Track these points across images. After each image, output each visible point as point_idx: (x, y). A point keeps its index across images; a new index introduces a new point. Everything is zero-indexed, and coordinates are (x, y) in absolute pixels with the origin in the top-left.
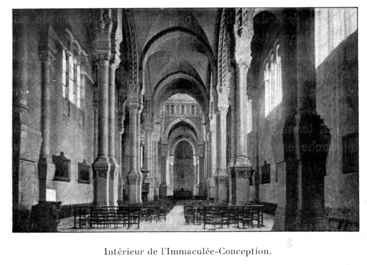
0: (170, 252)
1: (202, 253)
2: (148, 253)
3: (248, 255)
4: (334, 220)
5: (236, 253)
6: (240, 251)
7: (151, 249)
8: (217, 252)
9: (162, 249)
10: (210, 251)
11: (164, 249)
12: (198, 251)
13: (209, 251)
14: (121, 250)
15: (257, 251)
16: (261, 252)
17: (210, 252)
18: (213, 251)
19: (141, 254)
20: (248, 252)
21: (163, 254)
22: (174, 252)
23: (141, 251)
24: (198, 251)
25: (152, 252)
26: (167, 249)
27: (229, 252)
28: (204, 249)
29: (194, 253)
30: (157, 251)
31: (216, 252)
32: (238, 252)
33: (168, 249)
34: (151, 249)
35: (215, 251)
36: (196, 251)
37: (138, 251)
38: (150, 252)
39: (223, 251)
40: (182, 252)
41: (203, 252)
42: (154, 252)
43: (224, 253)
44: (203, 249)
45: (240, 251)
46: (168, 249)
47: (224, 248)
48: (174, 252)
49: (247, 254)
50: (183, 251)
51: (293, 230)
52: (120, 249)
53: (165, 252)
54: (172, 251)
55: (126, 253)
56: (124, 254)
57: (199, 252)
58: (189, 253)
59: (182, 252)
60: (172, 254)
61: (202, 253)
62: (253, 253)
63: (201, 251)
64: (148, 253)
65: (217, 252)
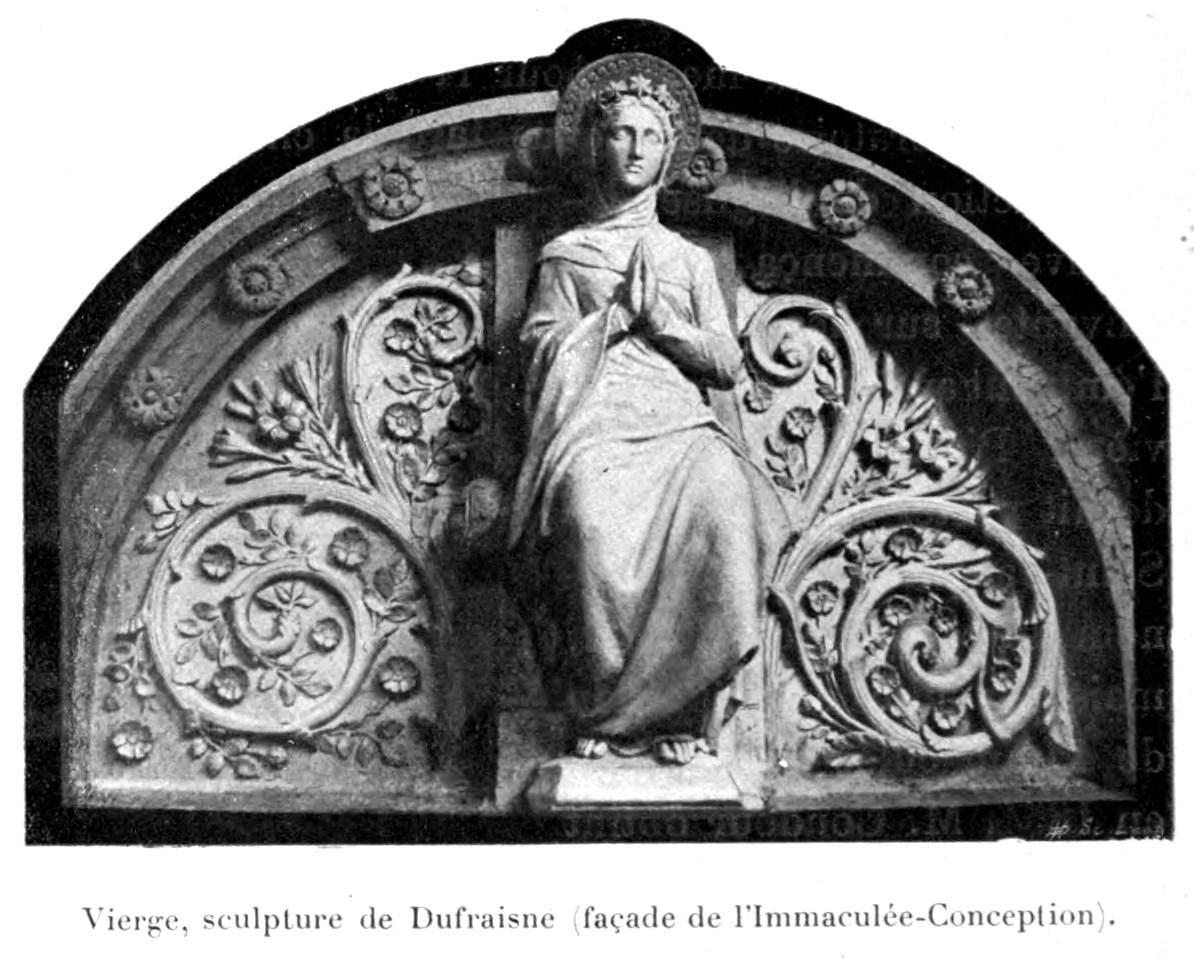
0: (764, 920)
1: (872, 920)
2: (691, 922)
3: (270, 931)
4: (966, 763)
5: (539, 922)
6: (998, 914)
7: (655, 909)
8: (923, 919)
9: (739, 908)
10: (899, 915)
11: (744, 910)
12: (857, 914)
13: (895, 916)
14: (893, 909)
15: (1053, 913)
16: (1067, 918)
17: (898, 919)
18: (910, 916)
19: (317, 926)
20: (1027, 918)
21: (739, 925)
22: (776, 919)
23: (317, 918)
24: (857, 914)
25: (702, 919)
26: (754, 910)
27: (1073, 918)
28: (256, 909)
29: (992, 921)
30: (340, 918)
31: (919, 919)
32: (994, 918)
33: (758, 908)
34: (655, 909)
35: (915, 917)
36: (850, 915)
37: (308, 917)
38: (696, 920)
39: (940, 915)
40: (803, 919)
41: (875, 918)
42: (381, 921)
43: (946, 923)
44: (254, 911)
45: (998, 914)
46: (758, 908)
47: (944, 905)
48: (776, 919)
49: (1022, 922)
50: (807, 916)
51: (796, 834)
52: (891, 905)
53: (749, 917)
54: (770, 916)
55: (324, 923)
56: (137, 928)
57: (862, 919)
58: (830, 920)
59: (803, 919)
60: (798, 924)
61: (872, 920)
62: (287, 926)
63: (867, 914)
64: (691, 922)
65: (923, 919)
